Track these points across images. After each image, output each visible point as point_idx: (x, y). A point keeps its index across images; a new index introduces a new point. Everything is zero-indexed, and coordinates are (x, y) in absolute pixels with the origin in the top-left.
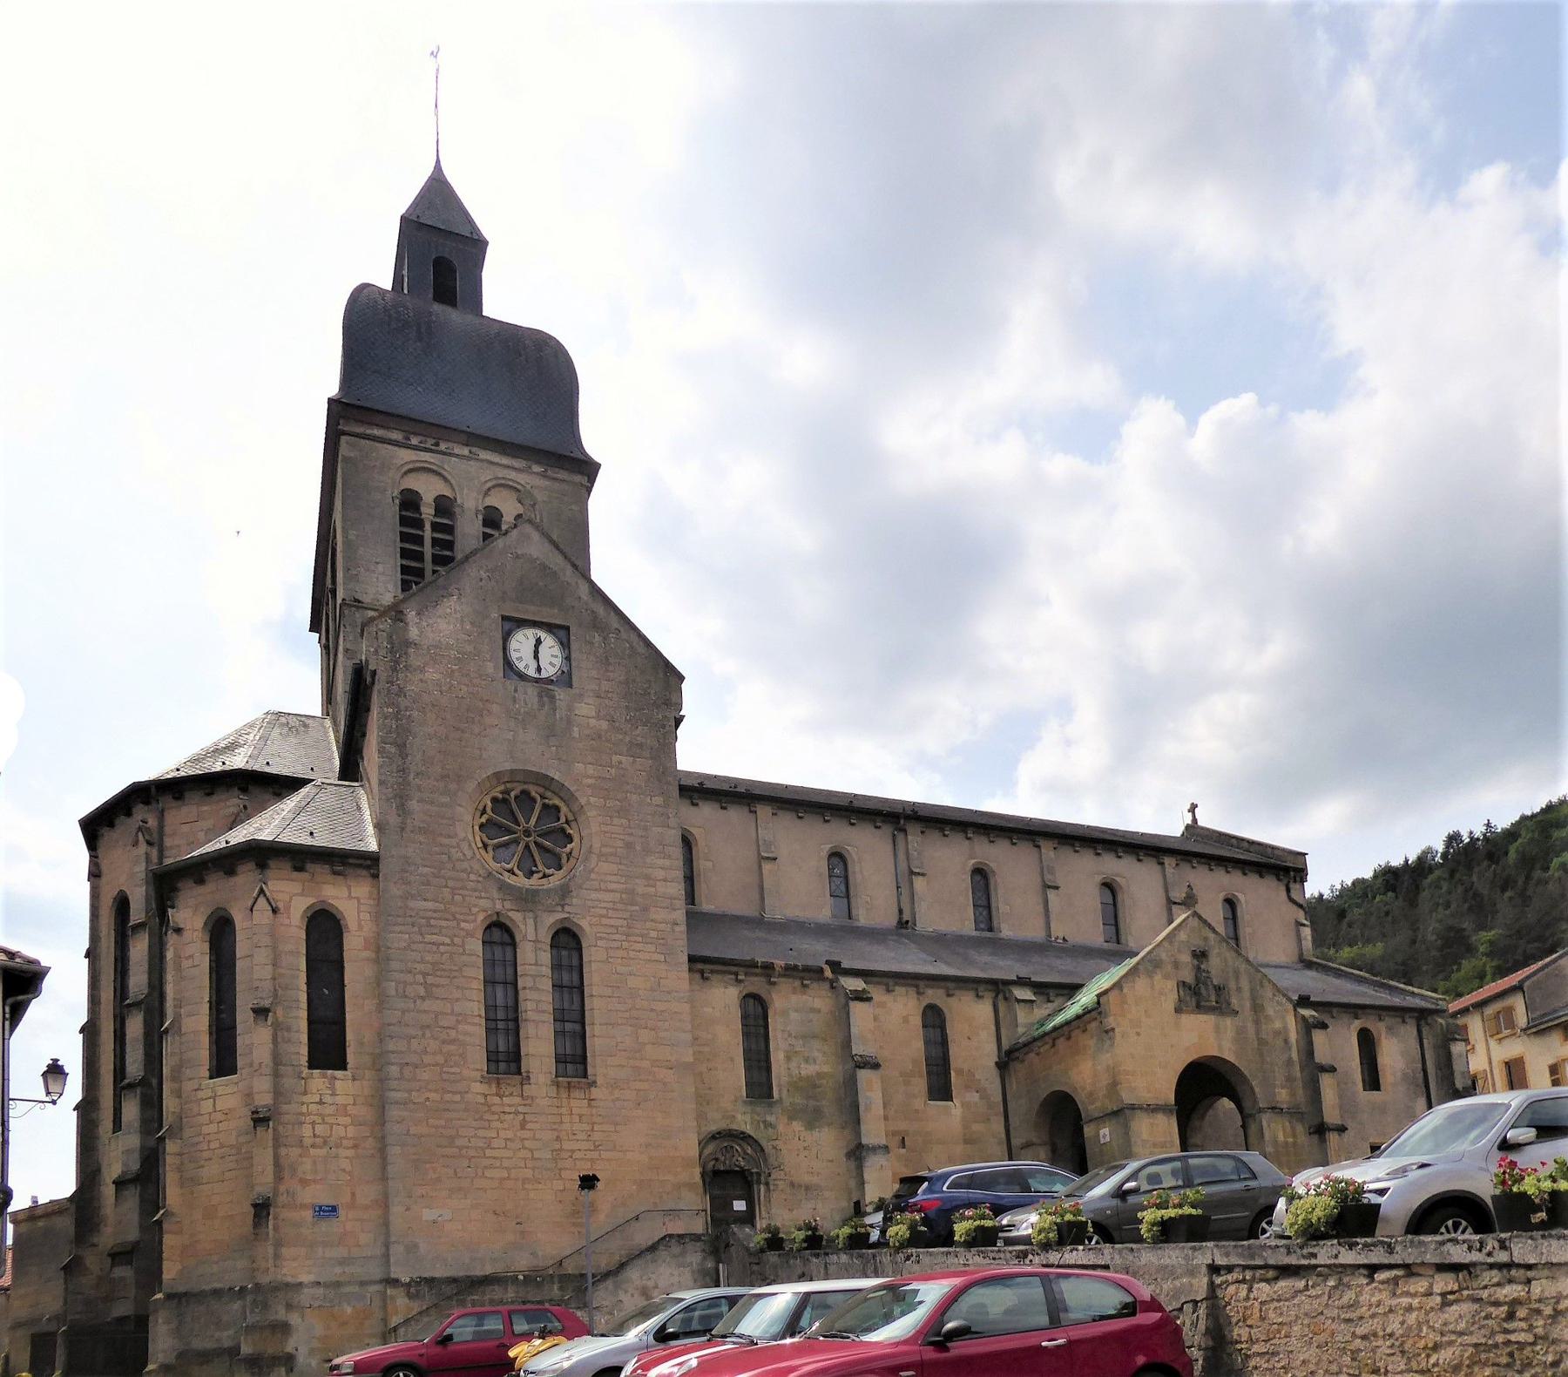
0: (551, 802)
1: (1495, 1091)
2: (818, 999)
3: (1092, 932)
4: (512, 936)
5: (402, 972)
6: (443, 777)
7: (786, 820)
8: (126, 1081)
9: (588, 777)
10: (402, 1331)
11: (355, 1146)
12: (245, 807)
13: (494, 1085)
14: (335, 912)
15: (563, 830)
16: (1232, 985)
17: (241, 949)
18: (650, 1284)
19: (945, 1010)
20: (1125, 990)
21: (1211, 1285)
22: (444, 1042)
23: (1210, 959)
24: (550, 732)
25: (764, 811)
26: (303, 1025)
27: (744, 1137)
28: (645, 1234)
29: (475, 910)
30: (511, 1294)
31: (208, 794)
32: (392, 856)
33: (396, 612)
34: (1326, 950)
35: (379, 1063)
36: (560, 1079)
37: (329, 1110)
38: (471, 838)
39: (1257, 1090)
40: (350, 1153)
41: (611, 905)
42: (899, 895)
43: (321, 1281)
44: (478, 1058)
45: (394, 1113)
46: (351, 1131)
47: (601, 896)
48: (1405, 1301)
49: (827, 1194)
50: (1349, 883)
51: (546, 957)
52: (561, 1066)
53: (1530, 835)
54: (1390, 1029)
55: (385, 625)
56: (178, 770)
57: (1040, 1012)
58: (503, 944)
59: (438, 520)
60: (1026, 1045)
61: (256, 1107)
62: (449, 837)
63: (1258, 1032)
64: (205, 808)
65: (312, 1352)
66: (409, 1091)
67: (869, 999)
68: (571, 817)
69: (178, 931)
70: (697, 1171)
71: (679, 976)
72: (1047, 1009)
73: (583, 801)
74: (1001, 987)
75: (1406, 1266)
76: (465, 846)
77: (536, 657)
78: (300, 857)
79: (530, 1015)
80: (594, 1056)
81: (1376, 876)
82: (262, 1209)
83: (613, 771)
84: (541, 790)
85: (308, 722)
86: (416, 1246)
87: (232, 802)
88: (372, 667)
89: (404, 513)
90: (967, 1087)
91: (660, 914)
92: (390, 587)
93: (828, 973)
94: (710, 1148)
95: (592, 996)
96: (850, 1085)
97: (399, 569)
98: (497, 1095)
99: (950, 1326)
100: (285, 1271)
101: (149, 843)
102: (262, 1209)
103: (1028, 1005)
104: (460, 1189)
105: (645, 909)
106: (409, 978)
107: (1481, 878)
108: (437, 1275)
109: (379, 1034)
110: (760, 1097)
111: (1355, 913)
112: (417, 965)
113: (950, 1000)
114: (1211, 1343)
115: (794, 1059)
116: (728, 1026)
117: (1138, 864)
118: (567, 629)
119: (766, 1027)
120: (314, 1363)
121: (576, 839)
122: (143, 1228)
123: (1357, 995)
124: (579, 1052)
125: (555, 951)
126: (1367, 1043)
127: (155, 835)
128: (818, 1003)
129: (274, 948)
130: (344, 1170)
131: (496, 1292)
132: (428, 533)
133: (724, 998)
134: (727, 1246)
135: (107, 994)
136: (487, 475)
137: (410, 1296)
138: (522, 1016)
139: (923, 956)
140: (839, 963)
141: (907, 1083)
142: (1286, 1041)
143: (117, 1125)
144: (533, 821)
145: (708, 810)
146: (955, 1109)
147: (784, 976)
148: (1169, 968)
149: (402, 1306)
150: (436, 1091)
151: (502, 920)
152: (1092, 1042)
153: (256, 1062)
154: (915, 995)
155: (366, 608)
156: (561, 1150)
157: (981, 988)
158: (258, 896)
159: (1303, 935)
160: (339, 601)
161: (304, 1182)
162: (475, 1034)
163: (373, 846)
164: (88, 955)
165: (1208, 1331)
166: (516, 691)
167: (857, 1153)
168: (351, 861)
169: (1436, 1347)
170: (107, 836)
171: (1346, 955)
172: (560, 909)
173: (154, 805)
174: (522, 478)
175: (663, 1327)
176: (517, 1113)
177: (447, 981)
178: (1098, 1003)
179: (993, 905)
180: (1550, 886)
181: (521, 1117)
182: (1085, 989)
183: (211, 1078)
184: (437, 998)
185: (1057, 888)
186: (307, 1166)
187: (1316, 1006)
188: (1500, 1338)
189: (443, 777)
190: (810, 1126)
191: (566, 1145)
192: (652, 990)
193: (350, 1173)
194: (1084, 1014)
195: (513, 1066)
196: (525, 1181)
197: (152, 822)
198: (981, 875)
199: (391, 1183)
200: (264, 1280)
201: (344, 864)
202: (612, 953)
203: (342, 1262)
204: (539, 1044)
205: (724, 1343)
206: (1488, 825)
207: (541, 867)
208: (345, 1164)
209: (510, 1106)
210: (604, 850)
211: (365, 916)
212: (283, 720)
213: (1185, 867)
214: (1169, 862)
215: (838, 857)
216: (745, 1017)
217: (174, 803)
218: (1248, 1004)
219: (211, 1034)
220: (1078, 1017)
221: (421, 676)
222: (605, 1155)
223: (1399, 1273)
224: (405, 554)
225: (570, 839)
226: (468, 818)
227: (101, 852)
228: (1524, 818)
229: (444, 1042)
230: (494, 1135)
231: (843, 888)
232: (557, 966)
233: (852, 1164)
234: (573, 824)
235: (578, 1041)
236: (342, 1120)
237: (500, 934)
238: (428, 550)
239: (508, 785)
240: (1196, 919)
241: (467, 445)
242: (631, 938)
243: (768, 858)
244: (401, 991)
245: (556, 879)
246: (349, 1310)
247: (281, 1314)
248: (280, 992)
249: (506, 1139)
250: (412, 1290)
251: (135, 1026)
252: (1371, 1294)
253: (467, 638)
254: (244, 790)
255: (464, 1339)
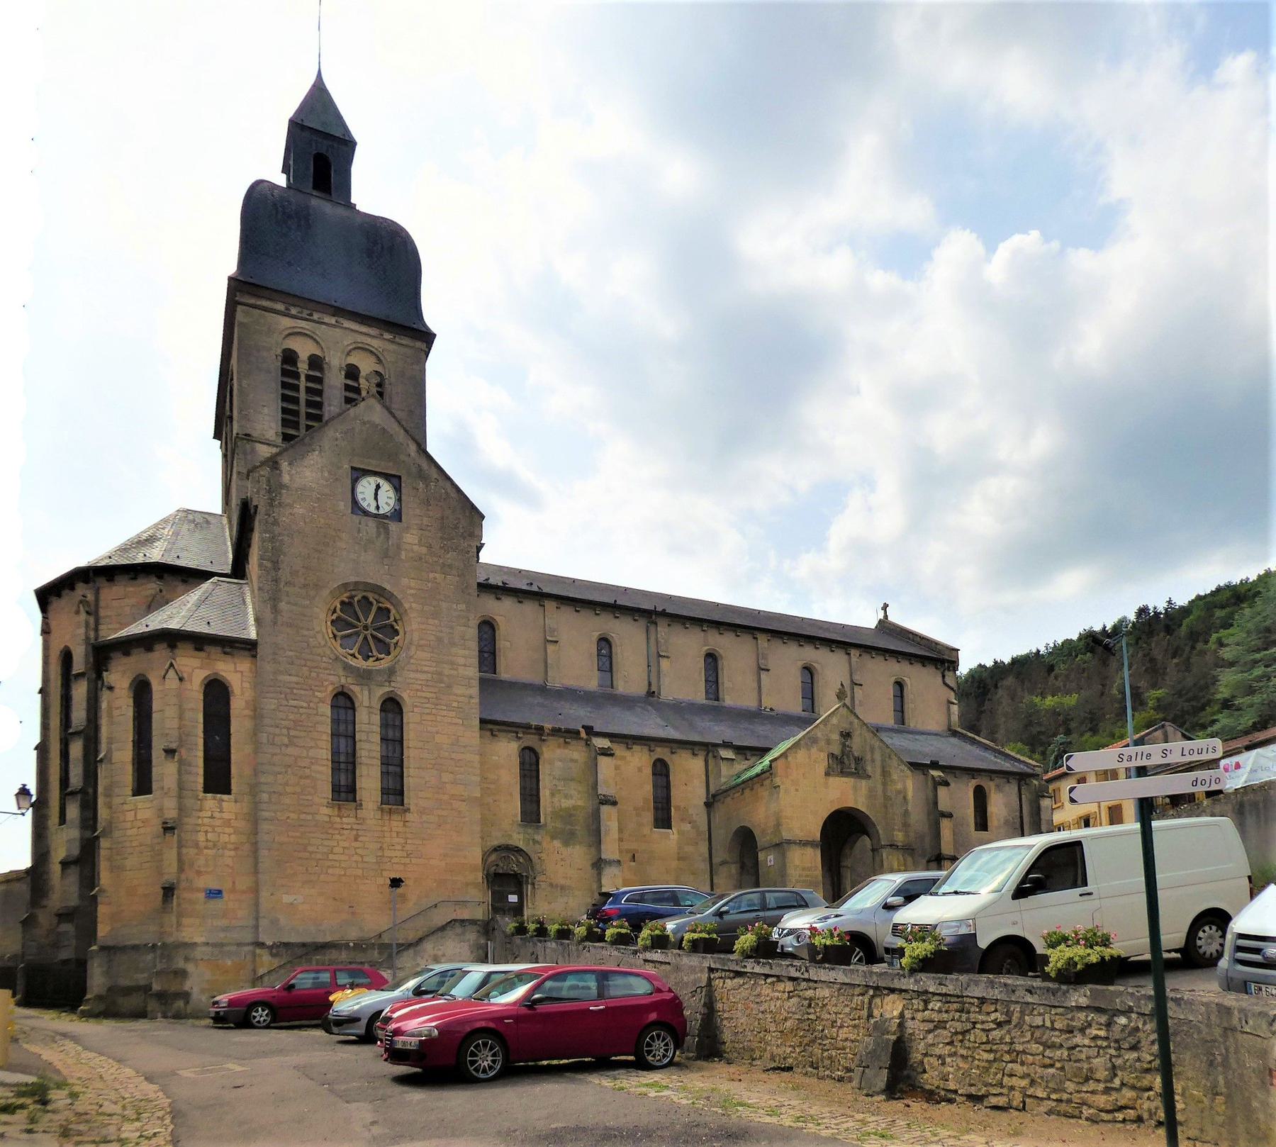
0: (384, 606)
1: (1101, 825)
2: (576, 753)
3: (794, 705)
4: (353, 703)
5: (272, 726)
6: (305, 586)
7: (567, 614)
8: (70, 789)
9: (411, 588)
10: (266, 979)
11: (236, 849)
12: (161, 591)
13: (336, 809)
14: (221, 679)
15: (392, 627)
16: (868, 757)
17: (156, 705)
18: (440, 953)
19: (669, 763)
20: (790, 759)
21: (709, 979)
22: (301, 777)
23: (854, 738)
24: (386, 555)
25: (550, 605)
26: (200, 762)
27: (518, 851)
28: (440, 918)
29: (326, 683)
30: (344, 956)
31: (132, 579)
32: (266, 643)
33: (273, 463)
34: (1034, 697)
35: (254, 789)
36: (384, 806)
37: (218, 823)
38: (324, 631)
39: (880, 832)
40: (232, 853)
41: (423, 683)
42: (649, 672)
43: (210, 942)
44: (326, 790)
45: (264, 826)
46: (233, 839)
47: (419, 676)
48: (777, 994)
49: (577, 893)
50: (1060, 642)
51: (377, 718)
52: (385, 796)
53: (1199, 613)
54: (997, 786)
55: (265, 471)
56: (110, 557)
57: (740, 766)
58: (346, 708)
59: (311, 373)
60: (726, 791)
61: (166, 819)
62: (308, 629)
63: (884, 791)
64: (131, 589)
65: (203, 991)
66: (275, 812)
67: (612, 755)
68: (398, 617)
69: (111, 688)
70: (480, 875)
71: (472, 735)
72: (745, 764)
73: (407, 606)
74: (710, 748)
75: (778, 977)
76: (319, 637)
77: (376, 498)
78: (200, 642)
79: (364, 760)
80: (409, 790)
81: (1080, 639)
82: (169, 891)
83: (429, 585)
84: (377, 597)
85: (210, 519)
86: (278, 920)
87: (151, 586)
88: (255, 503)
89: (285, 366)
90: (682, 820)
91: (459, 690)
92: (273, 425)
93: (583, 735)
94: (493, 857)
95: (409, 747)
96: (596, 817)
97: (280, 410)
98: (338, 816)
99: (536, 996)
100: (184, 934)
101: (88, 613)
102: (169, 891)
103: (730, 762)
104: (311, 881)
105: (449, 686)
106: (277, 731)
107: (1158, 644)
108: (292, 940)
109: (255, 770)
110: (532, 821)
111: (1061, 668)
112: (283, 722)
113: (674, 756)
114: (706, 1011)
115: (557, 795)
116: (510, 770)
117: (831, 654)
118: (399, 477)
119: (538, 771)
120: (204, 998)
121: (401, 633)
122: (81, 897)
123: (982, 760)
124: (398, 787)
125: (383, 714)
126: (981, 798)
127: (93, 608)
128: (576, 755)
129: (180, 707)
130: (228, 866)
131: (333, 954)
132: (303, 383)
133: (507, 750)
134: (494, 929)
135: (55, 722)
136: (348, 340)
137: (273, 955)
138: (358, 760)
139: (659, 720)
140: (592, 728)
141: (638, 815)
142: (905, 798)
143: (63, 819)
144: (370, 620)
145: (508, 603)
146: (673, 835)
147: (553, 735)
148: (822, 743)
149: (266, 962)
150: (294, 812)
151: (345, 690)
152: (766, 794)
153: (166, 787)
154: (647, 752)
155: (252, 441)
156: (383, 856)
157: (696, 748)
158: (169, 668)
159: (952, 711)
160: (234, 435)
161: (199, 873)
162: (323, 773)
163: (253, 635)
164: (41, 691)
165: (705, 1005)
166: (360, 523)
167: (599, 864)
168: (237, 645)
169: (786, 1019)
170: (56, 604)
171: (1048, 703)
172: (387, 684)
173: (91, 585)
174: (376, 343)
175: (419, 986)
176: (352, 829)
177: (302, 734)
178: (771, 766)
179: (720, 681)
180: (1207, 657)
181: (355, 832)
182: (772, 751)
183: (134, 795)
184: (297, 746)
185: (768, 670)
186: (201, 861)
187: (942, 768)
188: (806, 1017)
189: (305, 586)
190: (566, 843)
191: (387, 853)
192: (453, 745)
193: (232, 868)
194: (762, 773)
195: (351, 796)
196: (356, 877)
197: (90, 597)
198: (712, 659)
199: (260, 876)
200: (170, 940)
201: (231, 647)
202: (425, 717)
203: (225, 929)
204: (369, 781)
205: (440, 999)
206: (1170, 602)
207: (375, 653)
208: (229, 861)
209: (348, 824)
210: (422, 642)
211: (247, 685)
212: (191, 517)
213: (866, 657)
214: (854, 652)
215: (604, 642)
216: (522, 764)
217: (106, 584)
218: (879, 771)
219: (133, 764)
220: (758, 775)
221: (291, 511)
222: (414, 861)
223: (774, 979)
224: (285, 398)
225: (396, 633)
226: (323, 616)
227: (51, 615)
228: (1199, 598)
229: (301, 777)
230: (336, 844)
231: (607, 664)
232: (385, 725)
233: (595, 872)
234: (400, 623)
235: (398, 779)
236: (227, 830)
237: (343, 702)
238: (303, 396)
239: (353, 593)
240: (846, 709)
241: (334, 316)
242: (438, 707)
243: (551, 641)
244: (271, 740)
245: (386, 663)
246: (229, 963)
247: (181, 964)
248: (184, 738)
249: (344, 848)
250: (274, 951)
251: (76, 749)
252: (766, 990)
253: (325, 483)
254: (160, 577)
255: (305, 987)
